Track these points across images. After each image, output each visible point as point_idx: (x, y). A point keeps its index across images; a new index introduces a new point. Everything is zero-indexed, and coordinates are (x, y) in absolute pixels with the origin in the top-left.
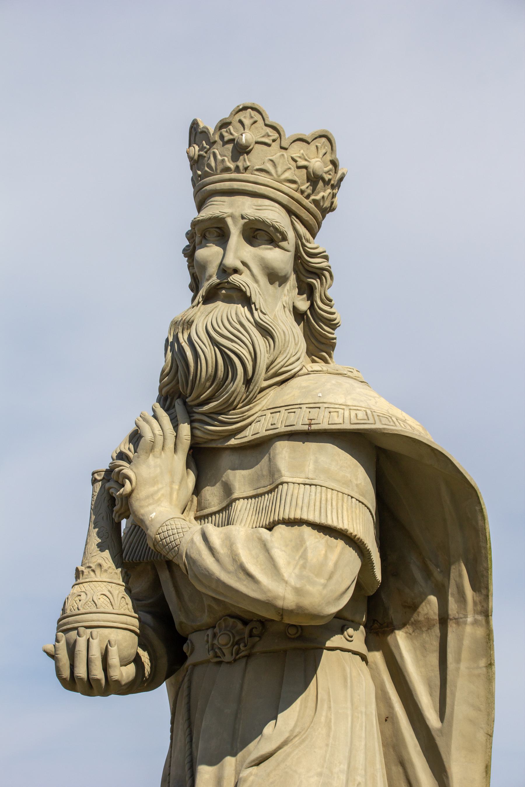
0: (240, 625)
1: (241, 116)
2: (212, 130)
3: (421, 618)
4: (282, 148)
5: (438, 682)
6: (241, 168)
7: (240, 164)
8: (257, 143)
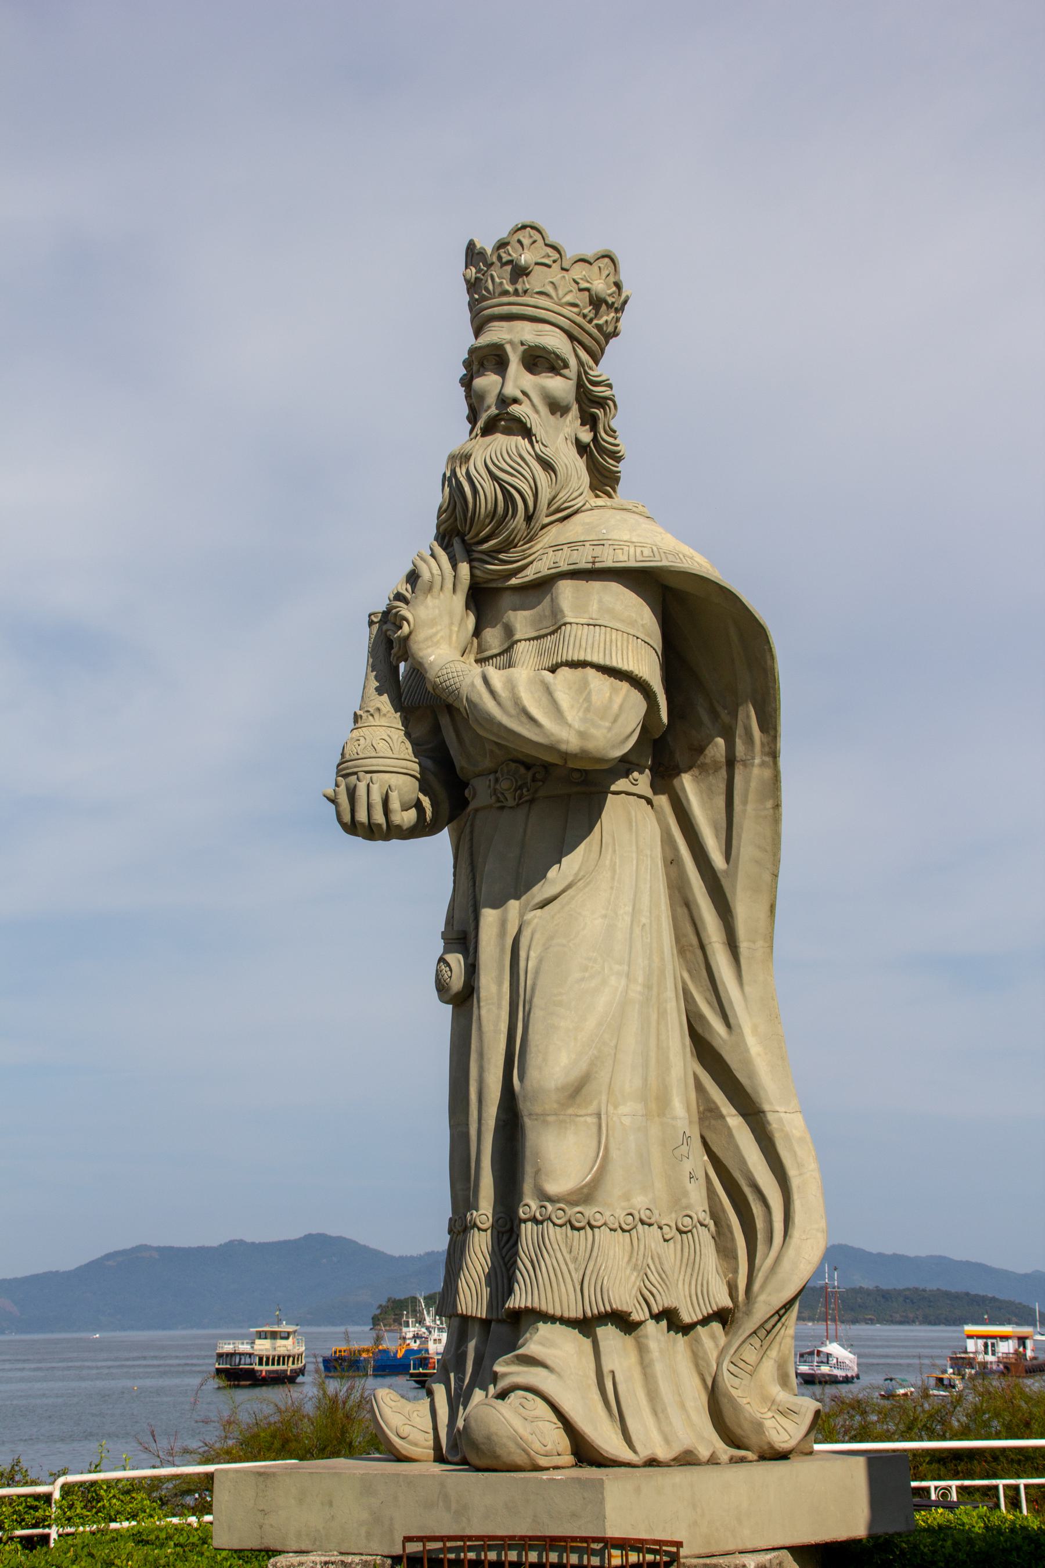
0: (522, 770)
1: (520, 235)
2: (489, 251)
3: (708, 761)
4: (563, 269)
5: (724, 825)
6: (520, 291)
7: (519, 287)
8: (537, 264)
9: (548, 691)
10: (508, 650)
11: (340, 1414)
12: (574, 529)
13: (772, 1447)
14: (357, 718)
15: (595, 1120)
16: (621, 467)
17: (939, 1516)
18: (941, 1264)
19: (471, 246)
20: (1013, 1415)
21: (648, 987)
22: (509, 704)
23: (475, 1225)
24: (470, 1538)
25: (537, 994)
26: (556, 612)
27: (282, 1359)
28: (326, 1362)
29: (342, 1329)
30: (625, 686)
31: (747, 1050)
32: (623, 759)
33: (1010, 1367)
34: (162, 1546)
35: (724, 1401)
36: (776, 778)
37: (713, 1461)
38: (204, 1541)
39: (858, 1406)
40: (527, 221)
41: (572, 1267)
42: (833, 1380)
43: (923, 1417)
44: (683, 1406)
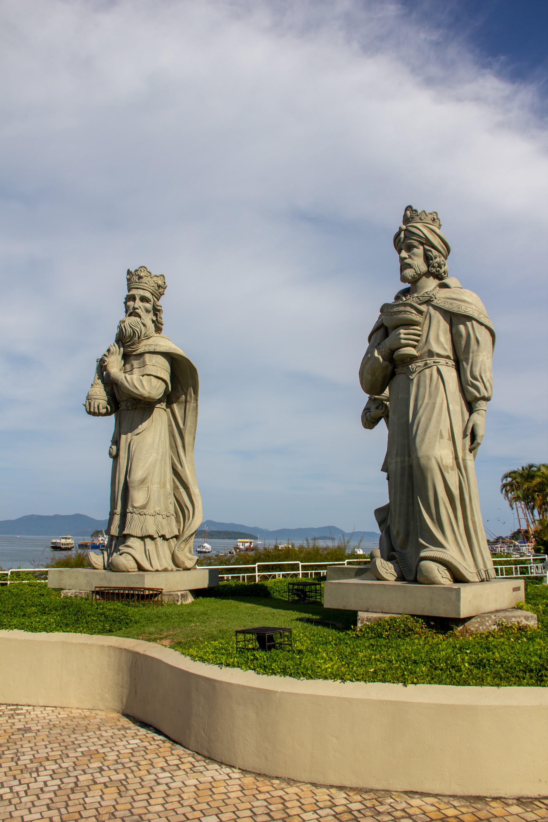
0: (134, 401)
1: (141, 269)
2: (133, 272)
3: (180, 401)
5: (183, 417)
7: (140, 281)
9: (141, 381)
10: (132, 370)
11: (81, 558)
12: (150, 341)
13: (186, 568)
14: (92, 385)
15: (147, 489)
16: (163, 327)
17: (225, 582)
18: (233, 525)
19: (129, 270)
20: (245, 560)
21: (162, 456)
22: (131, 384)
23: (116, 513)
24: (111, 587)
25: (134, 457)
26: (144, 362)
27: (68, 544)
28: (79, 545)
29: (83, 537)
30: (161, 381)
31: (186, 473)
32: (159, 399)
33: (247, 549)
34: (35, 587)
35: (175, 557)
36: (197, 406)
37: (172, 570)
38: (46, 586)
39: (209, 558)
40: (143, 266)
41: (140, 524)
42: (205, 552)
43: (224, 560)
44: (165, 558)
